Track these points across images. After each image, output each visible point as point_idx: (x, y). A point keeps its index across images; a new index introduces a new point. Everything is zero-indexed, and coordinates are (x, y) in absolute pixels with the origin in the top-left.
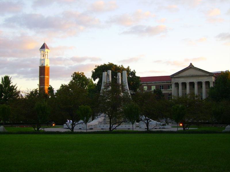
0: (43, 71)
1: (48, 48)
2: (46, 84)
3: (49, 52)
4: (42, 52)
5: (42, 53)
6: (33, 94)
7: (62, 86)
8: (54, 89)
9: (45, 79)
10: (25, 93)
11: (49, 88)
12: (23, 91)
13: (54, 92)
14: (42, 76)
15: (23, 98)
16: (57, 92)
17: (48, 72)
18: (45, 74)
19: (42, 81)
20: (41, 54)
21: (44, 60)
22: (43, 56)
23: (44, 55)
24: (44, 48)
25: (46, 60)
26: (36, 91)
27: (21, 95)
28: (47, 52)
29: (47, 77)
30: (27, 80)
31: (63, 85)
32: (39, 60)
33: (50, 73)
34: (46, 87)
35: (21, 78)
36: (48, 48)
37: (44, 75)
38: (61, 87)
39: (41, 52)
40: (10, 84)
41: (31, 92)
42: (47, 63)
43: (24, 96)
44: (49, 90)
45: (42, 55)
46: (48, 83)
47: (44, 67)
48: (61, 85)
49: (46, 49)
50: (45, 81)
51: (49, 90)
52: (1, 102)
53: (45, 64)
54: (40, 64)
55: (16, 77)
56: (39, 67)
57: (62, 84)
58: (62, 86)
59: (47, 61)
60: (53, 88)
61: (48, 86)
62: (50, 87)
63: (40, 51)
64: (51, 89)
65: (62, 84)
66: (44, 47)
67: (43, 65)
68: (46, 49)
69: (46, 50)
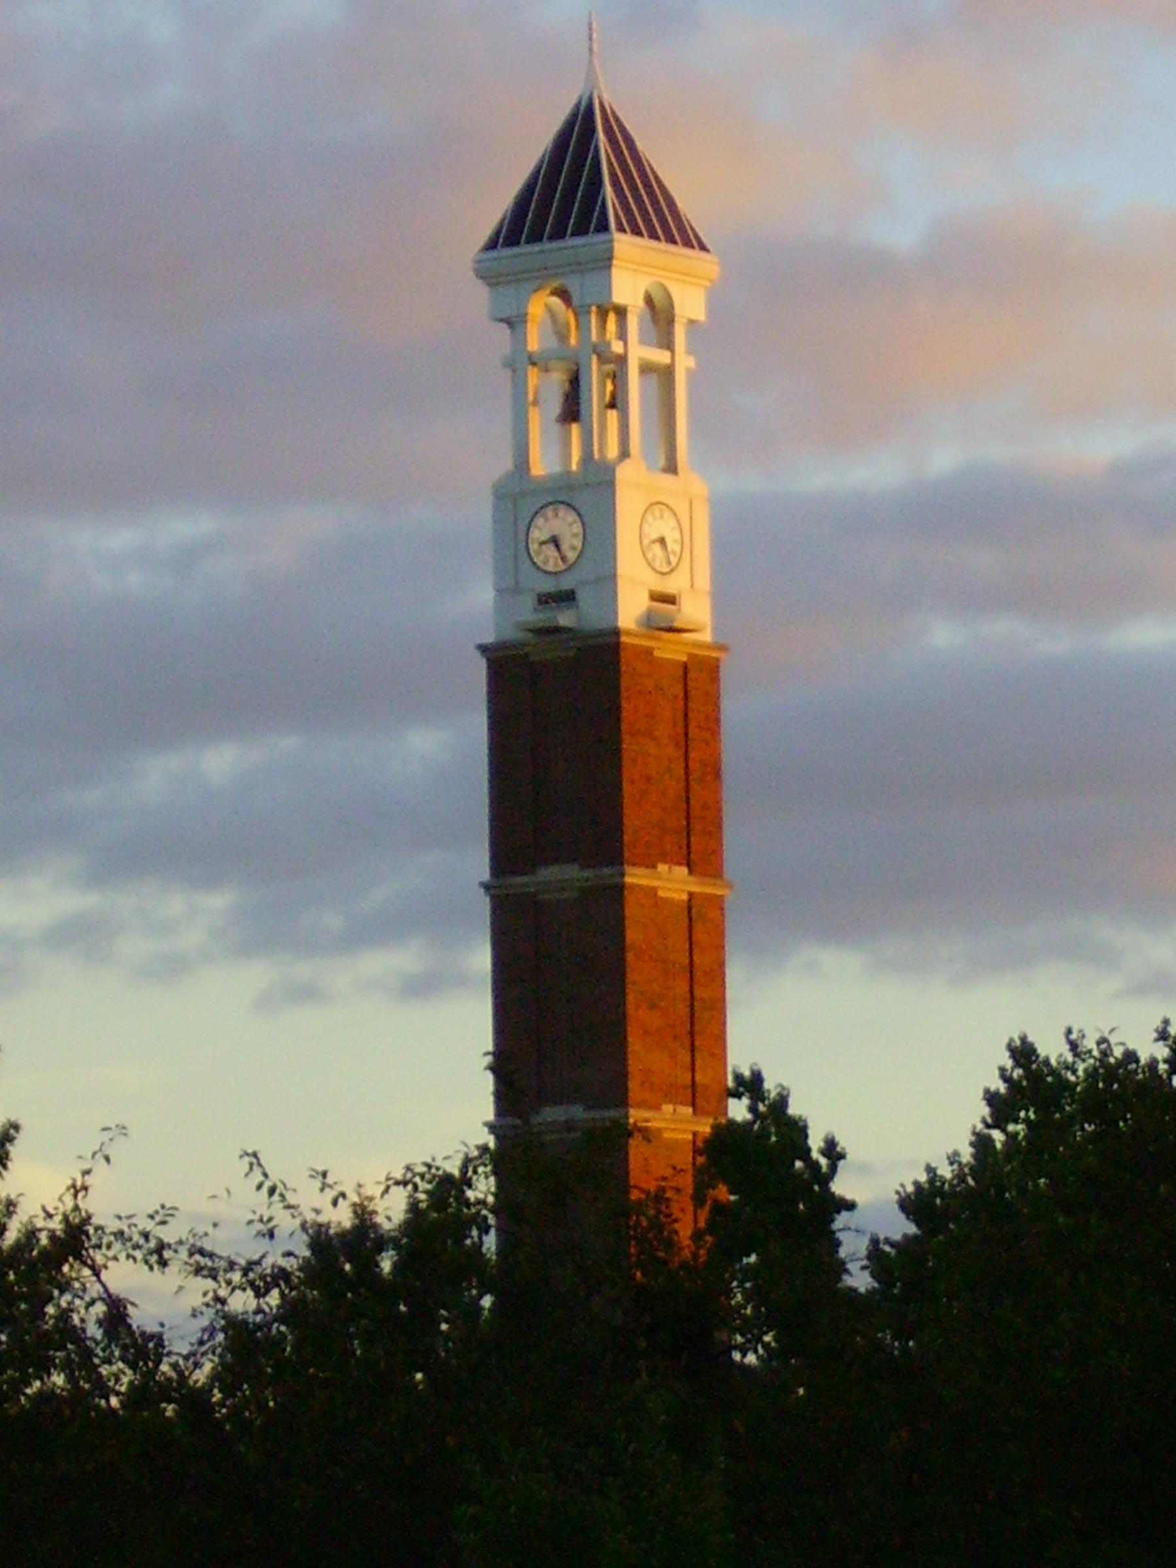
0: (583, 784)
1: (663, 222)
2: (645, 1056)
3: (690, 304)
4: (541, 306)
5: (534, 343)
6: (353, 1296)
7: (1030, 1084)
8: (832, 1150)
9: (633, 935)
10: (205, 1263)
11: (725, 1150)
12: (163, 1215)
13: (852, 1248)
14: (560, 877)
15: (166, 1391)
16: (902, 1227)
17: (698, 767)
18: (637, 820)
19: (574, 990)
20: (520, 363)
21: (589, 493)
22: (572, 411)
23: (596, 390)
24: (591, 220)
25: (635, 485)
26: (441, 1202)
27: (116, 1313)
28: (660, 315)
29: (672, 882)
30: (265, 1003)
31: (1052, 1049)
32: (480, 515)
33: (739, 840)
34: (669, 1128)
35: (171, 968)
36: (663, 222)
37: (606, 846)
38: (1001, 1108)
39: (515, 322)
40: (874, 1288)
41: (321, 1240)
42: (662, 560)
43: (179, 1346)
44: (724, 1194)
45: (548, 388)
46: (700, 1021)
47: (602, 653)
48: (989, 1069)
49: (625, 245)
50: (639, 977)
51: (724, 1194)
52: (444, 1242)
53: (608, 580)
54: (507, 592)
55: (79, 937)
56: (480, 667)
57: (1023, 1053)
58: (1030, 1084)
59: (663, 526)
60: (815, 1142)
61: (694, 1096)
62: (738, 1110)
63: (480, 294)
64: (771, 1168)
65: (1023, 1053)
66: (578, 192)
67: (565, 619)
68: (625, 245)
69: (634, 269)
